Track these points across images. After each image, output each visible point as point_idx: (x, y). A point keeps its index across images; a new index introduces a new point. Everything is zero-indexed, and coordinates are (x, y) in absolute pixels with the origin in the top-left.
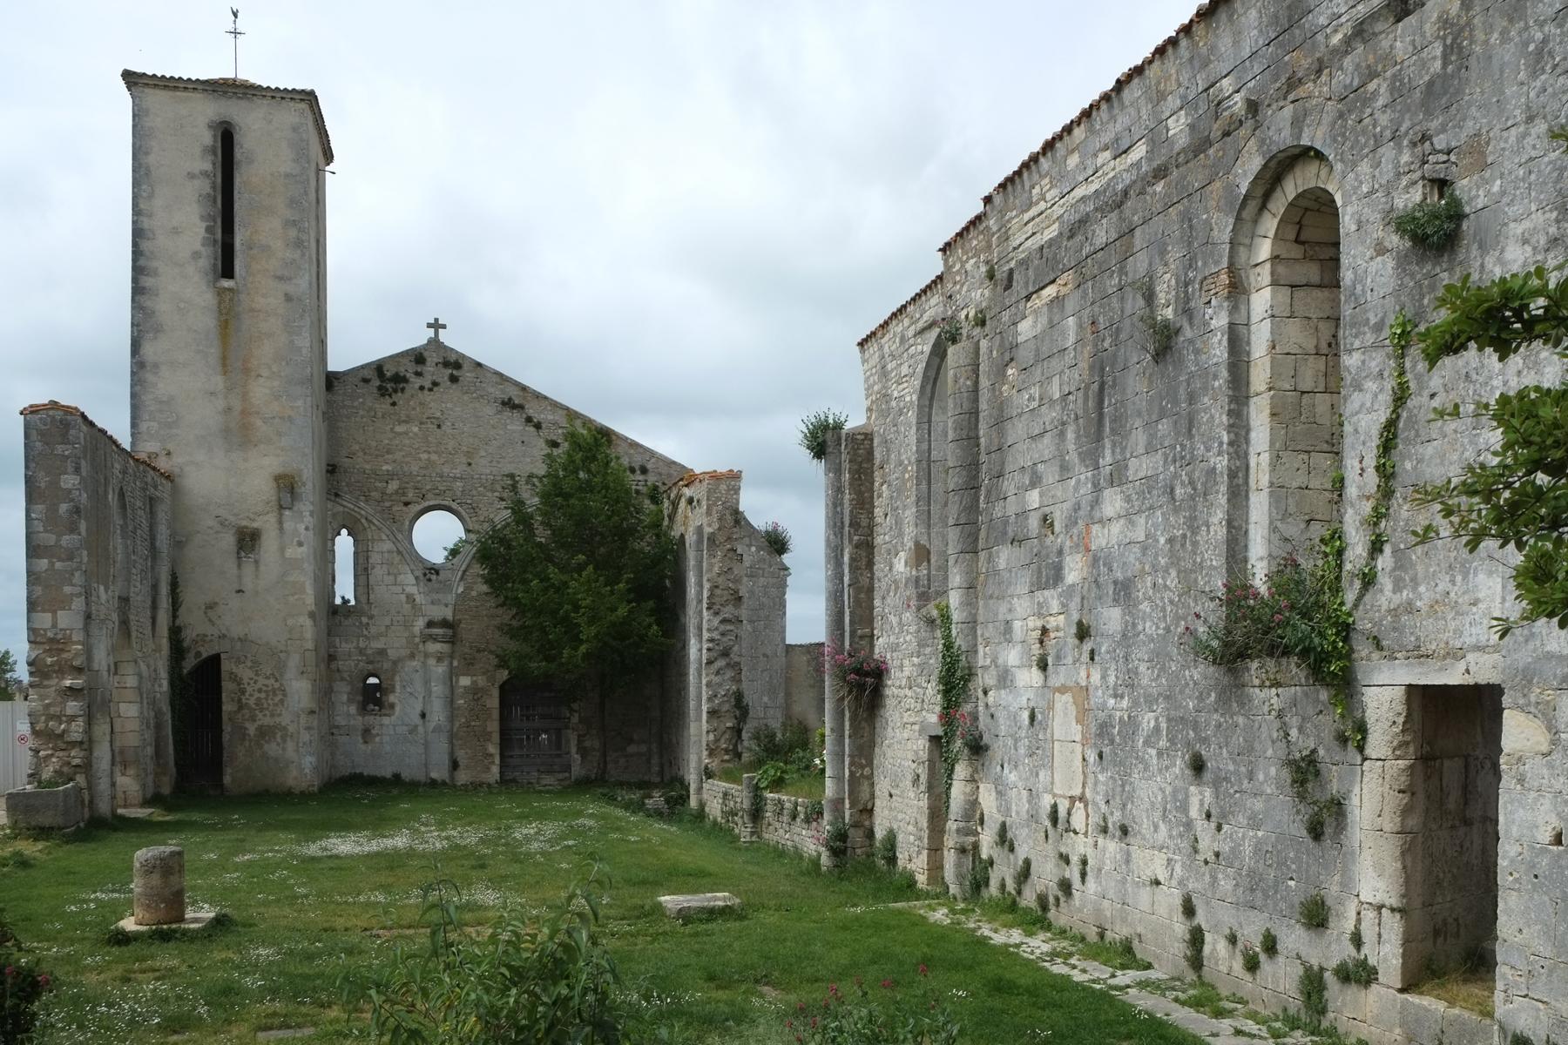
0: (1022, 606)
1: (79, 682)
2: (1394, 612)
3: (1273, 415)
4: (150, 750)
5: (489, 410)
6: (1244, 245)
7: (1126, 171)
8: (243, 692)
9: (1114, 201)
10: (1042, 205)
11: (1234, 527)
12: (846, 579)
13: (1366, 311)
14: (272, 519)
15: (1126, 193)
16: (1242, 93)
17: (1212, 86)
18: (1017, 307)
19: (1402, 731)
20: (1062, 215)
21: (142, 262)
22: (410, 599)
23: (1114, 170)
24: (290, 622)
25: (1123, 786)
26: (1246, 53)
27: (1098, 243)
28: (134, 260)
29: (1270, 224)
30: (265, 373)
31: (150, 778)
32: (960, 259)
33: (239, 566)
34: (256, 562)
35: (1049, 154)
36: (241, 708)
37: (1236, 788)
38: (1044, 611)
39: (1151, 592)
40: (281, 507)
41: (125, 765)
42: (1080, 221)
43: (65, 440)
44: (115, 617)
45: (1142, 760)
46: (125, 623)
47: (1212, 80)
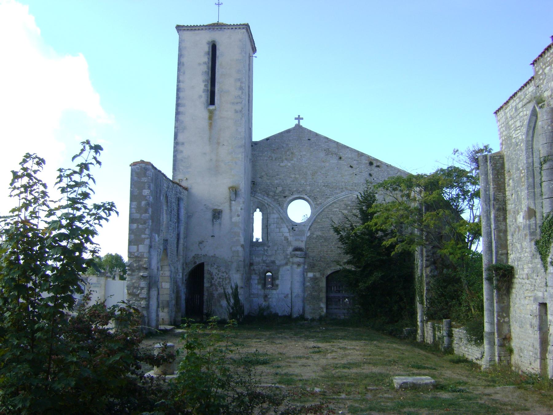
1: (146, 274)
4: (174, 302)
12: (493, 226)
21: (180, 102)
22: (286, 239)
24: (234, 249)
31: (174, 313)
32: (541, 68)
33: (213, 224)
34: (220, 224)
36: (212, 285)
40: (231, 200)
41: (163, 308)
43: (145, 175)
44: (161, 247)
46: (165, 249)
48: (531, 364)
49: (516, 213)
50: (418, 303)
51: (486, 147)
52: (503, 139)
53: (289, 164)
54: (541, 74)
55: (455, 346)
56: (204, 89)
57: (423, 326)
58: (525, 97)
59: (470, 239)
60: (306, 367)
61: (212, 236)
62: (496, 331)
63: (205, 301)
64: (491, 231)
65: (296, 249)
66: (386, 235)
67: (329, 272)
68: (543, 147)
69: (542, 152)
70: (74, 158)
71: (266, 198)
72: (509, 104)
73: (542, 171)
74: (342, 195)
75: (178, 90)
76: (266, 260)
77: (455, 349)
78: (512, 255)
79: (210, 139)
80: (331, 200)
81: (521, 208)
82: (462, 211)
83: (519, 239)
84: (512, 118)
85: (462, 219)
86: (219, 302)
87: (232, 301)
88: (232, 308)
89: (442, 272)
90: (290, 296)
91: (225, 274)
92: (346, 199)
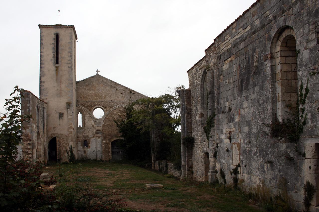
0: (225, 126)
2: (312, 127)
3: (282, 85)
5: (108, 88)
6: (274, 48)
7: (246, 32)
8: (61, 144)
9: (243, 39)
10: (227, 41)
11: (273, 109)
13: (303, 62)
14: (66, 111)
15: (246, 37)
16: (272, 14)
17: (265, 13)
18: (222, 63)
19: (315, 153)
20: (232, 43)
21: (42, 62)
22: (93, 126)
23: (242, 32)
24: (69, 130)
25: (249, 163)
26: (272, 5)
27: (240, 48)
28: (40, 62)
29: (279, 43)
30: (64, 82)
34: (63, 119)
35: (228, 29)
36: (60, 147)
37: (275, 164)
38: (230, 127)
39: (254, 124)
40: (67, 109)
42: (236, 44)
44: (37, 130)
45: (253, 158)
47: (265, 12)
48: (201, 177)
49: (196, 115)
50: (152, 154)
51: (182, 86)
52: (191, 83)
53: (94, 92)
54: (209, 56)
55: (169, 171)
56: (53, 56)
57: (154, 162)
58: (201, 65)
59: (175, 125)
60: (107, 182)
61: (60, 125)
62: (186, 164)
63: (57, 154)
64: (185, 123)
65: (98, 130)
66: (138, 124)
67: (112, 140)
68: (209, 88)
69: (208, 90)
70: (11, 94)
71: (83, 107)
72: (194, 68)
73: (208, 98)
74: (117, 106)
75: (41, 56)
76: (84, 135)
77: (169, 172)
78: (193, 133)
79: (57, 80)
80: (113, 108)
81: (198, 113)
82: (171, 114)
83: (196, 126)
84: (195, 74)
85: (171, 117)
86: (64, 154)
87: (70, 154)
88: (70, 157)
89: (163, 140)
90: (95, 151)
91: (66, 142)
92: (119, 108)
